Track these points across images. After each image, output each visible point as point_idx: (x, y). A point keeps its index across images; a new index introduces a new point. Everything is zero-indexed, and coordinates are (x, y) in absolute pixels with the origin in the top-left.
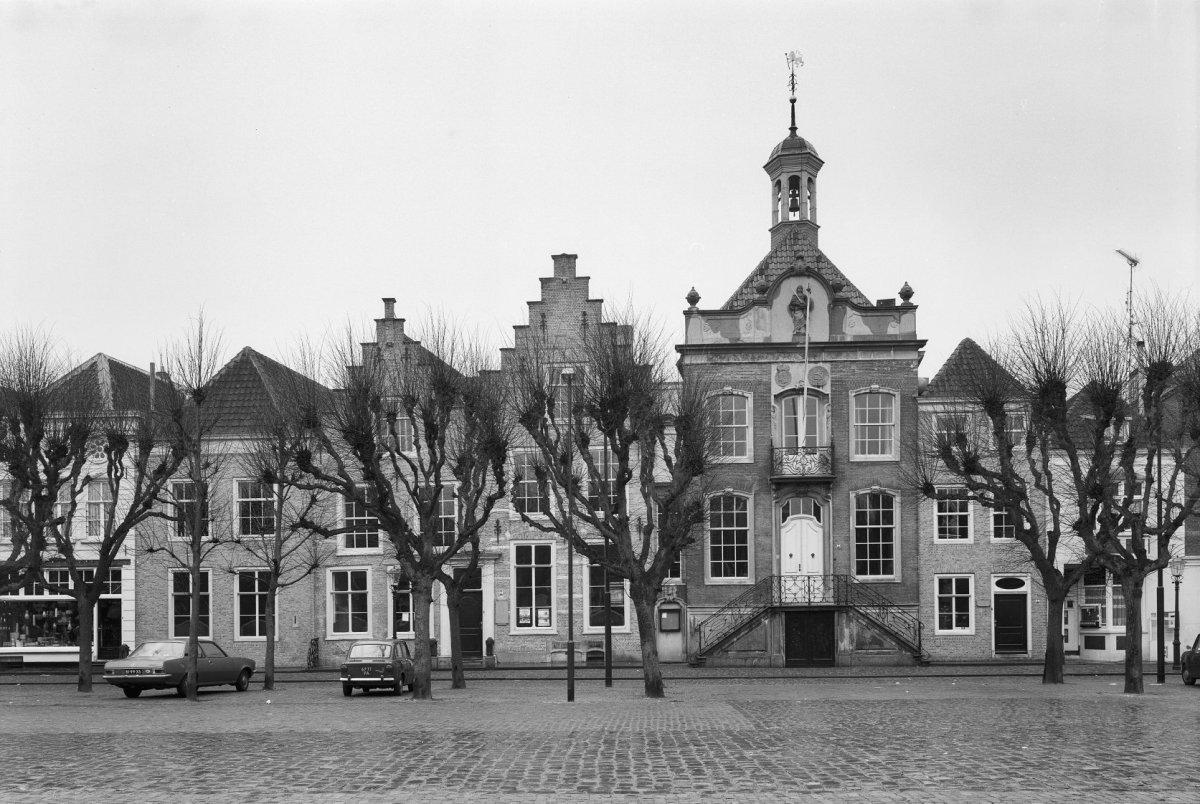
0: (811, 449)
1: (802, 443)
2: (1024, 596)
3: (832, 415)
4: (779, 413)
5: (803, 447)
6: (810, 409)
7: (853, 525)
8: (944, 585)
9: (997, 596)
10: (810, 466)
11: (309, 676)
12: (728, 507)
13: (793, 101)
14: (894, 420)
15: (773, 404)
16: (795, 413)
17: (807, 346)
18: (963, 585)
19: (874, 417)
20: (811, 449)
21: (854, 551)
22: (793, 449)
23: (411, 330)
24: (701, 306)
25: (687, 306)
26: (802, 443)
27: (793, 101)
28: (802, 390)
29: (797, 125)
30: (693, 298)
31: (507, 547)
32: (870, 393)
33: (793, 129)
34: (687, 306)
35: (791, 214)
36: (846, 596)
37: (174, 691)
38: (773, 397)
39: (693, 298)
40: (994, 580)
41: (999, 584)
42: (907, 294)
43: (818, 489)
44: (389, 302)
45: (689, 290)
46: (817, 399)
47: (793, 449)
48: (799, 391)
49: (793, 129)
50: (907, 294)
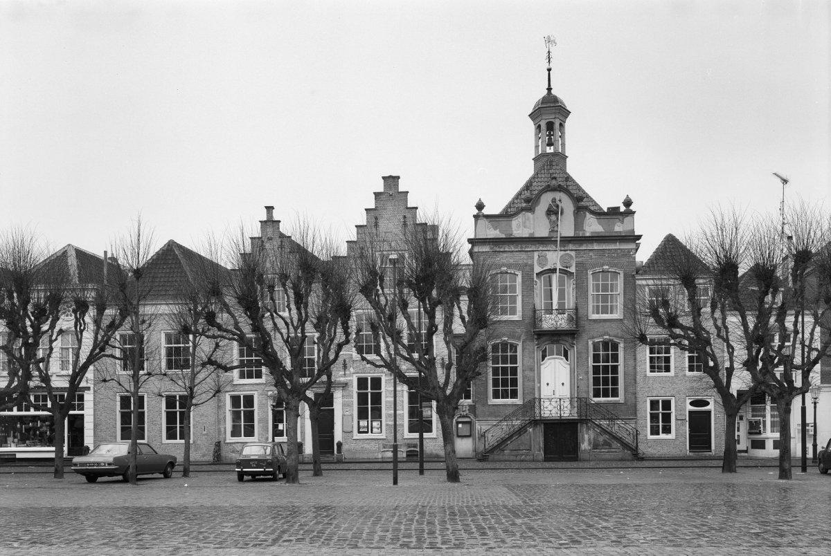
0: (561, 310)
1: (555, 306)
2: (709, 412)
3: (576, 287)
4: (540, 286)
5: (556, 309)
6: (561, 283)
7: (591, 363)
8: (654, 404)
9: (690, 412)
10: (561, 322)
11: (214, 467)
12: (504, 350)
13: (549, 70)
14: (619, 290)
15: (535, 279)
16: (551, 286)
17: (559, 239)
18: (667, 405)
19: (605, 288)
20: (561, 310)
21: (591, 381)
22: (549, 310)
23: (285, 228)
24: (485, 211)
25: (476, 212)
26: (555, 306)
27: (549, 70)
28: (556, 269)
29: (552, 87)
30: (480, 206)
31: (351, 378)
32: (603, 271)
33: (549, 89)
34: (476, 212)
35: (548, 148)
36: (586, 412)
37: (120, 478)
38: (535, 275)
39: (480, 206)
40: (688, 401)
41: (692, 404)
42: (628, 203)
43: (567, 338)
44: (270, 209)
45: (477, 201)
46: (566, 276)
47: (549, 310)
48: (553, 271)
49: (549, 89)
50: (628, 203)
